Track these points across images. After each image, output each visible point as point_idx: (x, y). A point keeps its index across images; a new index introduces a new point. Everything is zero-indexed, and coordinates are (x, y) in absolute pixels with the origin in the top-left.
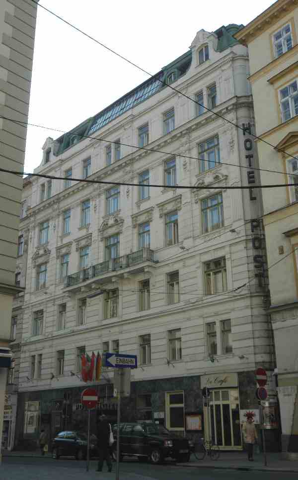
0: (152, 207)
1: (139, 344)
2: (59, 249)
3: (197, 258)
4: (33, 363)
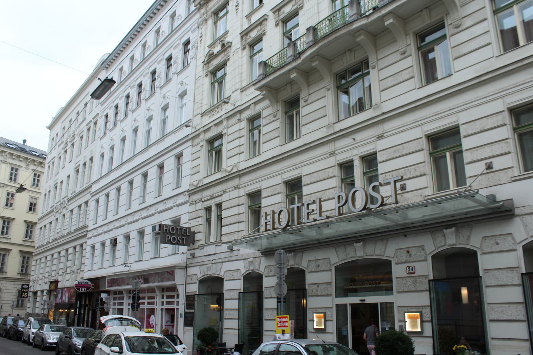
0: (265, 15)
1: (248, 206)
2: (245, 34)
3: (202, 137)
4: (209, 221)
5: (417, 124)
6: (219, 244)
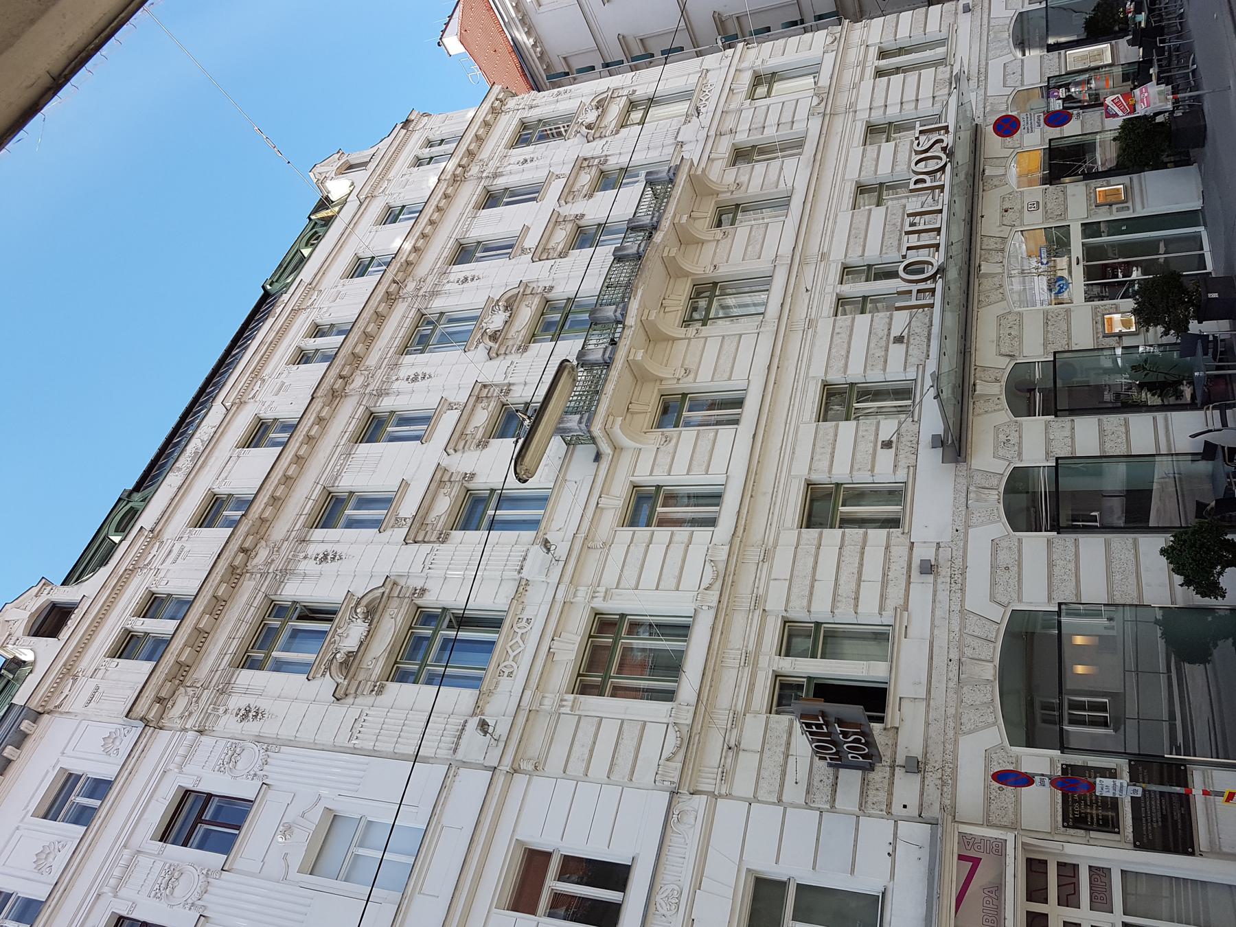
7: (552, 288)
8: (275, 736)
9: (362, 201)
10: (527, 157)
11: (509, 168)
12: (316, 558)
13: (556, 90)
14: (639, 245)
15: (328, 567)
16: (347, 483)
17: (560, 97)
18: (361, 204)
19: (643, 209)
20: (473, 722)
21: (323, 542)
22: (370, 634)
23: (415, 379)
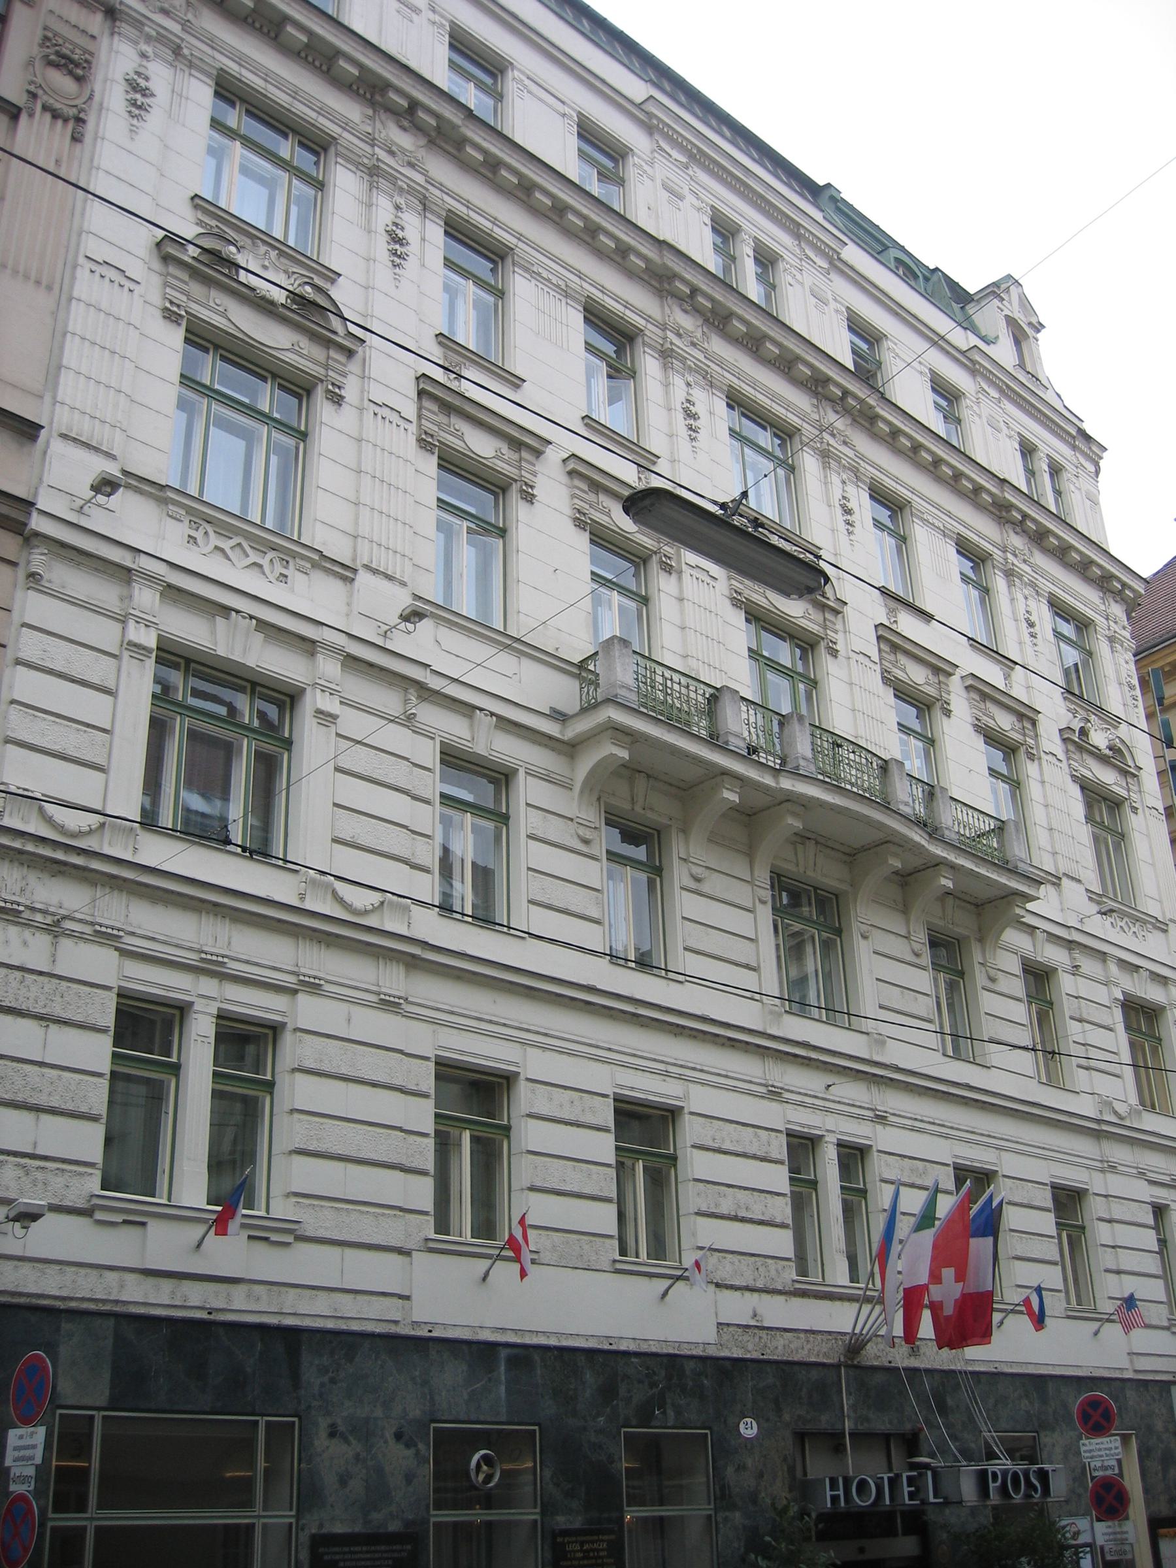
5: (945, 1133)
6: (274, 1237)
7: (834, 653)
8: (100, 134)
9: (968, 354)
10: (1037, 629)
11: (1020, 597)
12: (396, 224)
13: (1135, 682)
14: (906, 804)
15: (381, 246)
16: (521, 288)
17: (1127, 688)
18: (963, 353)
19: (962, 815)
20: (113, 469)
21: (423, 239)
22: (265, 306)
23: (690, 415)
